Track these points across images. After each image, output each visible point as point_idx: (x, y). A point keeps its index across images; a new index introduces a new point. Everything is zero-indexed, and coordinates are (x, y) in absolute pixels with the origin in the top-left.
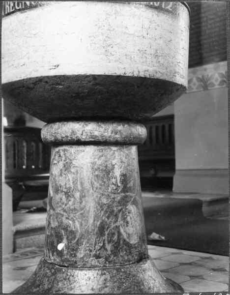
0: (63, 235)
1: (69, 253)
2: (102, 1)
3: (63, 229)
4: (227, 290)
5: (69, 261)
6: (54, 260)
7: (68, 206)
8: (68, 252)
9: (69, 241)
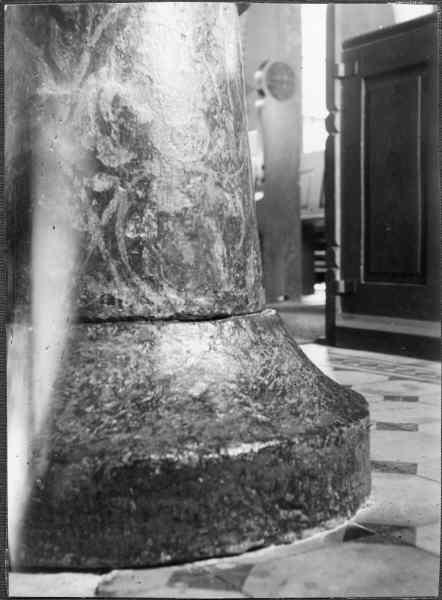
0: (211, 231)
1: (232, 279)
2: (5, 372)
3: (209, 214)
4: (206, 45)
5: (235, 299)
6: (189, 303)
7: (216, 150)
8: (230, 274)
9: (230, 246)
